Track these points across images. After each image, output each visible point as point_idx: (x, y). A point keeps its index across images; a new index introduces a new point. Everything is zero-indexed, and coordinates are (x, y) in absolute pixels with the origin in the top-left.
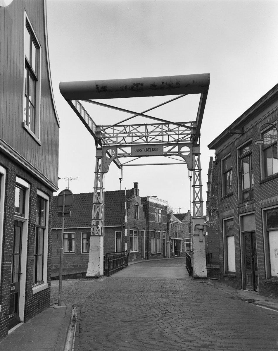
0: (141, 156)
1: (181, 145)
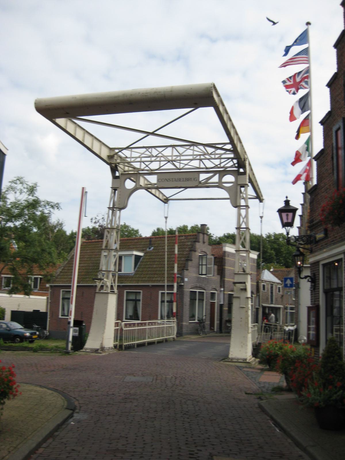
0: (186, 188)
1: (224, 172)
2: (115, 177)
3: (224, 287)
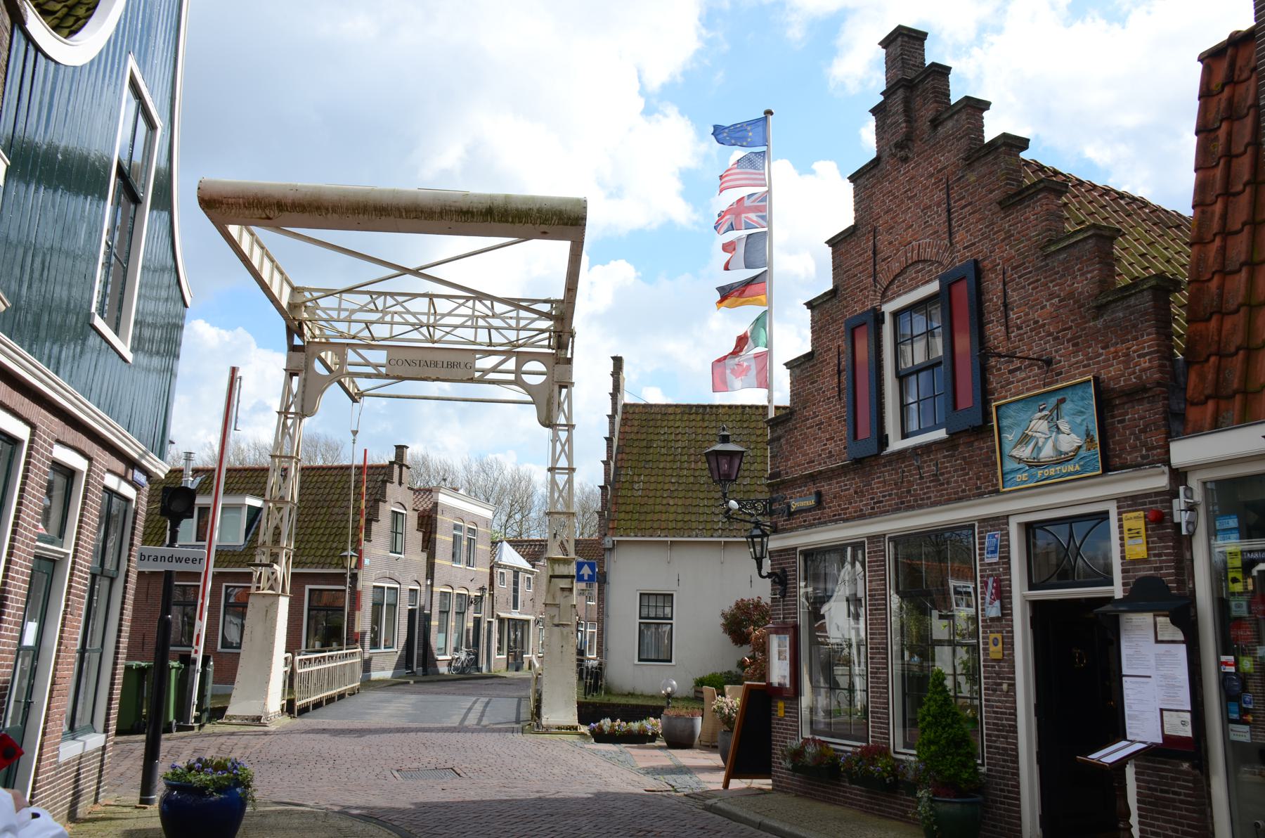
2: (293, 348)
3: (432, 579)
